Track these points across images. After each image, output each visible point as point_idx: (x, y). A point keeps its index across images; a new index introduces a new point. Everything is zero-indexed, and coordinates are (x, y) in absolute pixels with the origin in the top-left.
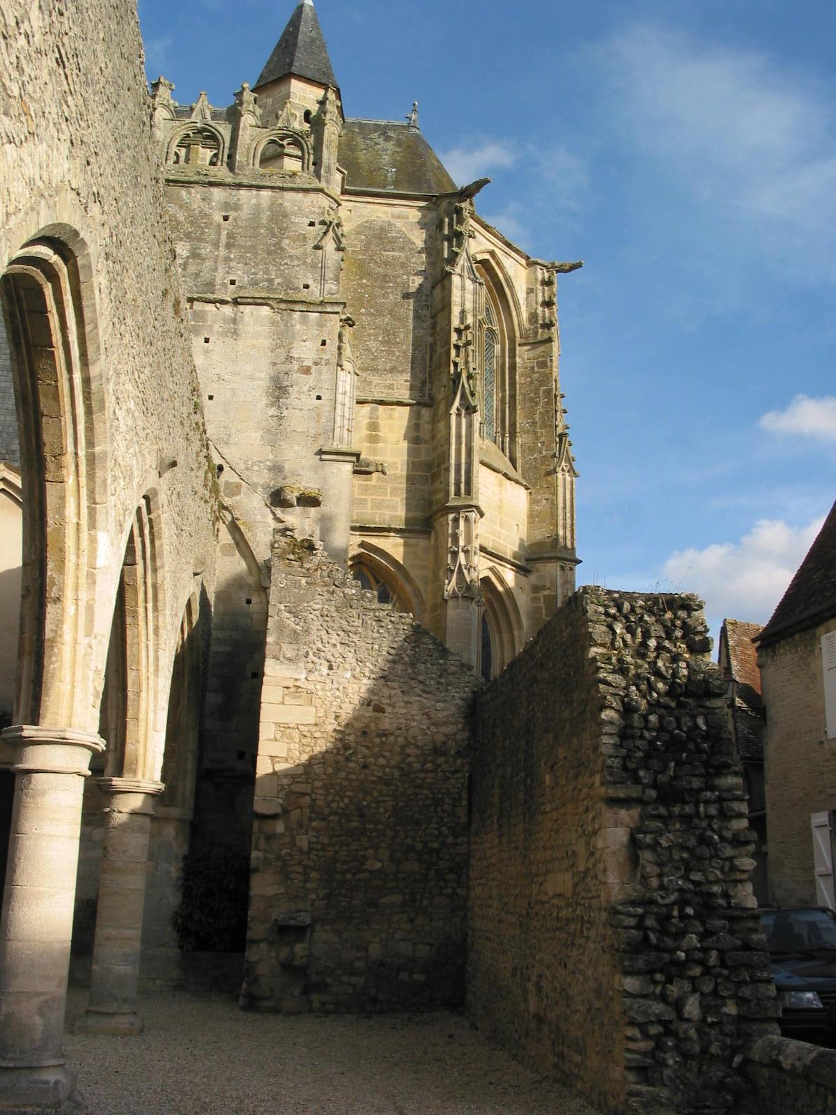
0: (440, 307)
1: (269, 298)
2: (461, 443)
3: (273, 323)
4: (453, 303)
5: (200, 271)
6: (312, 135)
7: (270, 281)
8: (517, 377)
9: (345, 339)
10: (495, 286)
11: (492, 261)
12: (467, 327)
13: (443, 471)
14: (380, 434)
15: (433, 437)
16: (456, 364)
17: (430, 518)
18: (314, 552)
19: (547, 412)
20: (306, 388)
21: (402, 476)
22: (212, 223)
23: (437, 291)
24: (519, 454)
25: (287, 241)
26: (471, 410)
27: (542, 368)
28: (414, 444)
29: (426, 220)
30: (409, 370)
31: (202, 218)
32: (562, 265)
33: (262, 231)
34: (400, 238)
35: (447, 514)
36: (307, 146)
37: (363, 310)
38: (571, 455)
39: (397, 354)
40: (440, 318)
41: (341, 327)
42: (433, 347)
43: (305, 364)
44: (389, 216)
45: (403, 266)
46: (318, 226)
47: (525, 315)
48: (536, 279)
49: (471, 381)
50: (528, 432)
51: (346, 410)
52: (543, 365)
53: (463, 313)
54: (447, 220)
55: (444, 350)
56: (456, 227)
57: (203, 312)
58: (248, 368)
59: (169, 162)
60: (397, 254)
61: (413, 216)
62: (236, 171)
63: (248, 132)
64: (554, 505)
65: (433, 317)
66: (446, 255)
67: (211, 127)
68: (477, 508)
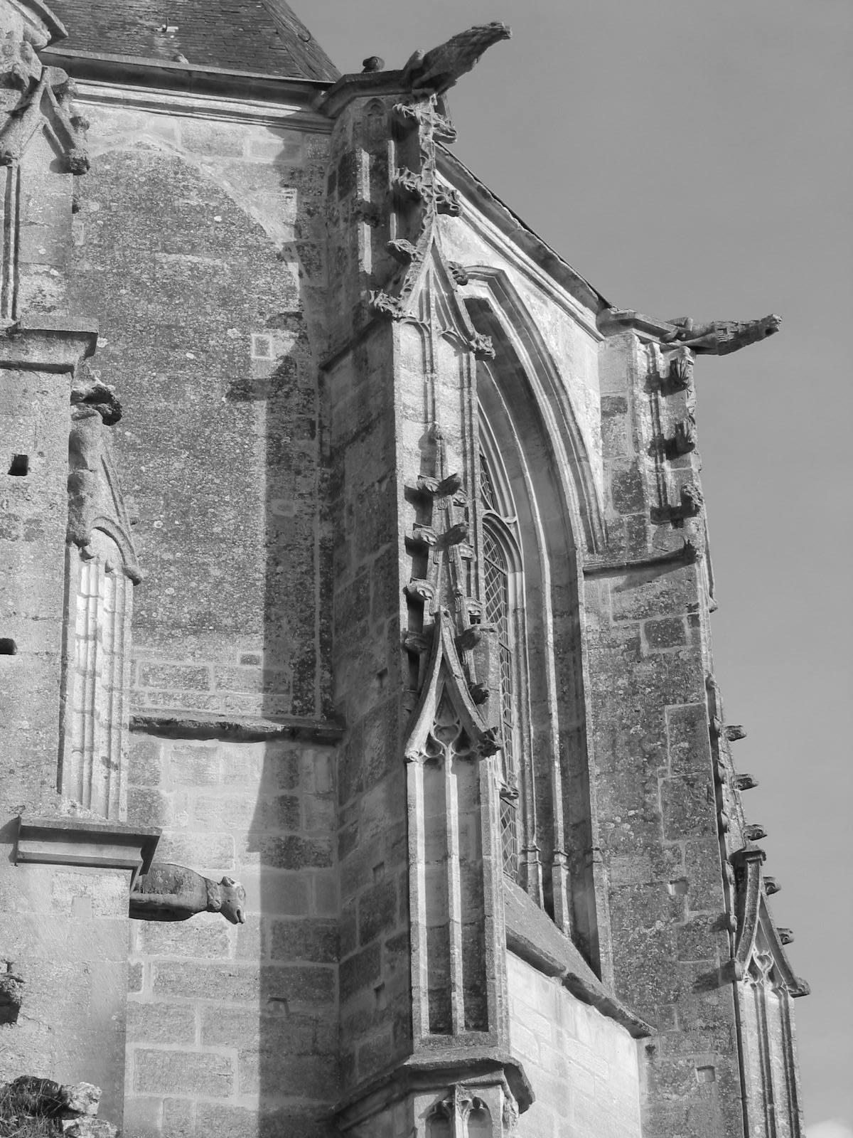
0: (353, 427)
2: (446, 856)
4: (398, 409)
8: (585, 674)
9: (93, 456)
10: (503, 387)
12: (449, 486)
13: (384, 951)
15: (345, 842)
17: (341, 1114)
18: (67, 1124)
19: (691, 783)
21: (241, 974)
23: (344, 375)
24: (603, 922)
26: (475, 747)
27: (665, 644)
29: (298, 161)
30: (258, 622)
32: (711, 330)
34: (216, 211)
35: (407, 1095)
38: (777, 923)
39: (215, 572)
40: (356, 464)
41: (75, 419)
42: (332, 553)
44: (178, 144)
45: (226, 299)
47: (600, 482)
48: (632, 370)
49: (469, 655)
50: (629, 849)
51: (101, 695)
52: (668, 634)
53: (432, 440)
54: (365, 158)
55: (370, 559)
60: (205, 261)
61: (256, 148)
64: (735, 1086)
65: (331, 458)
66: (367, 265)
68: (514, 1071)
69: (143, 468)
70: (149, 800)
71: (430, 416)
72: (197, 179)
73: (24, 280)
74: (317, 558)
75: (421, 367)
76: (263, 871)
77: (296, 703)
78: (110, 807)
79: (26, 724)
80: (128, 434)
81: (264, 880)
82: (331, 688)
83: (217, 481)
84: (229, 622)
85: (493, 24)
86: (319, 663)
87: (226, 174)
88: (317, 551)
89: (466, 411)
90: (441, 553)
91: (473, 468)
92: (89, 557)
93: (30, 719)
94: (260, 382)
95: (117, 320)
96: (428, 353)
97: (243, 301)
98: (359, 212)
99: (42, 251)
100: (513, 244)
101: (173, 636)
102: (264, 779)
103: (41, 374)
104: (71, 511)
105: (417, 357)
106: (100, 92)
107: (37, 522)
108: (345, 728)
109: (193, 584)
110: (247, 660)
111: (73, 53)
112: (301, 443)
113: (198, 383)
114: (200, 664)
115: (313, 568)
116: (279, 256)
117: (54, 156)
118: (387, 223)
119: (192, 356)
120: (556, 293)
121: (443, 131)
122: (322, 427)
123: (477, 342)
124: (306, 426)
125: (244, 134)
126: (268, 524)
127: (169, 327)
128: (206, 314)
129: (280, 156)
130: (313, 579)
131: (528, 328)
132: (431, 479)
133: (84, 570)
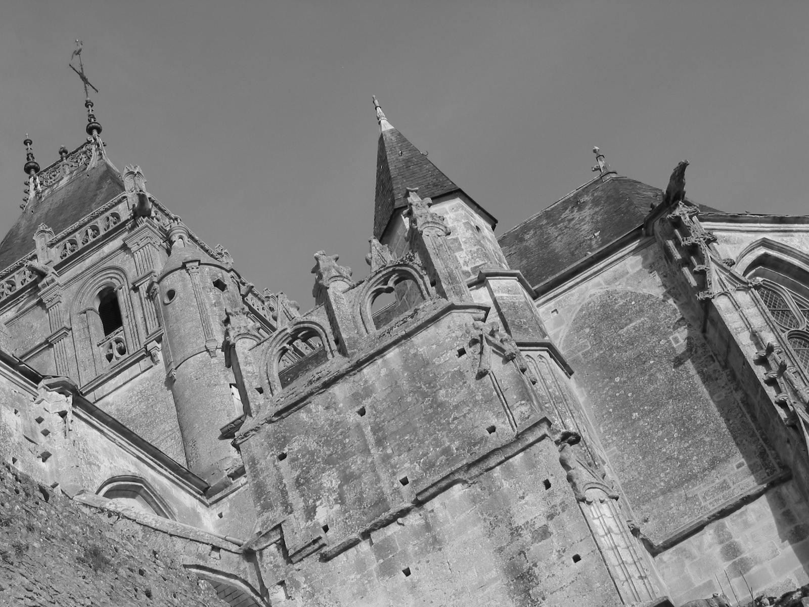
1: (453, 473)
3: (474, 500)
4: (733, 333)
5: (361, 493)
6: (416, 255)
7: (447, 451)
11: (770, 252)
14: (746, 555)
16: (783, 404)
20: (554, 556)
22: (349, 429)
23: (712, 332)
25: (442, 392)
28: (798, 541)
29: (650, 260)
30: (735, 448)
31: (336, 430)
33: (409, 399)
36: (416, 270)
37: (635, 415)
39: (707, 439)
42: (746, 402)
43: (537, 526)
44: (604, 286)
45: (653, 331)
46: (469, 351)
53: (755, 337)
54: (670, 243)
55: (759, 397)
56: (685, 243)
57: (387, 540)
58: (472, 576)
59: (275, 392)
60: (637, 322)
61: (633, 266)
62: (349, 352)
63: (345, 301)
65: (725, 366)
67: (303, 322)
69: (658, 417)
70: (732, 546)
71: (748, 326)
72: (618, 293)
73: (514, 412)
74: (744, 409)
75: (734, 309)
76: (793, 547)
77: (767, 471)
78: (651, 595)
79: (598, 585)
80: (646, 408)
81: (796, 551)
82: (777, 456)
83: (688, 403)
84: (723, 455)
85: (679, 164)
86: (767, 449)
87: (627, 284)
88: (741, 405)
89: (763, 313)
90: (782, 378)
91: (778, 334)
92: (591, 502)
93: (599, 582)
94: (683, 354)
95: (618, 367)
96: (733, 301)
97: (659, 327)
98: (679, 265)
99: (515, 397)
100: (762, 225)
101: (706, 475)
102: (773, 510)
103: (537, 444)
104: (574, 490)
105: (731, 306)
106: (566, 287)
107: (563, 502)
108: (791, 470)
109: (702, 449)
110: (739, 466)
111: (547, 281)
112: (711, 367)
113: (661, 370)
114: (722, 480)
115: (743, 413)
116: (664, 301)
117: (501, 359)
118: (691, 261)
119: (653, 362)
120: (794, 229)
121: (692, 213)
122: (716, 355)
123: (751, 283)
124: (709, 359)
125: (625, 264)
126: (717, 407)
127: (638, 357)
128: (649, 342)
129: (643, 263)
130: (746, 417)
131: (791, 251)
132: (761, 351)
133: (592, 508)
